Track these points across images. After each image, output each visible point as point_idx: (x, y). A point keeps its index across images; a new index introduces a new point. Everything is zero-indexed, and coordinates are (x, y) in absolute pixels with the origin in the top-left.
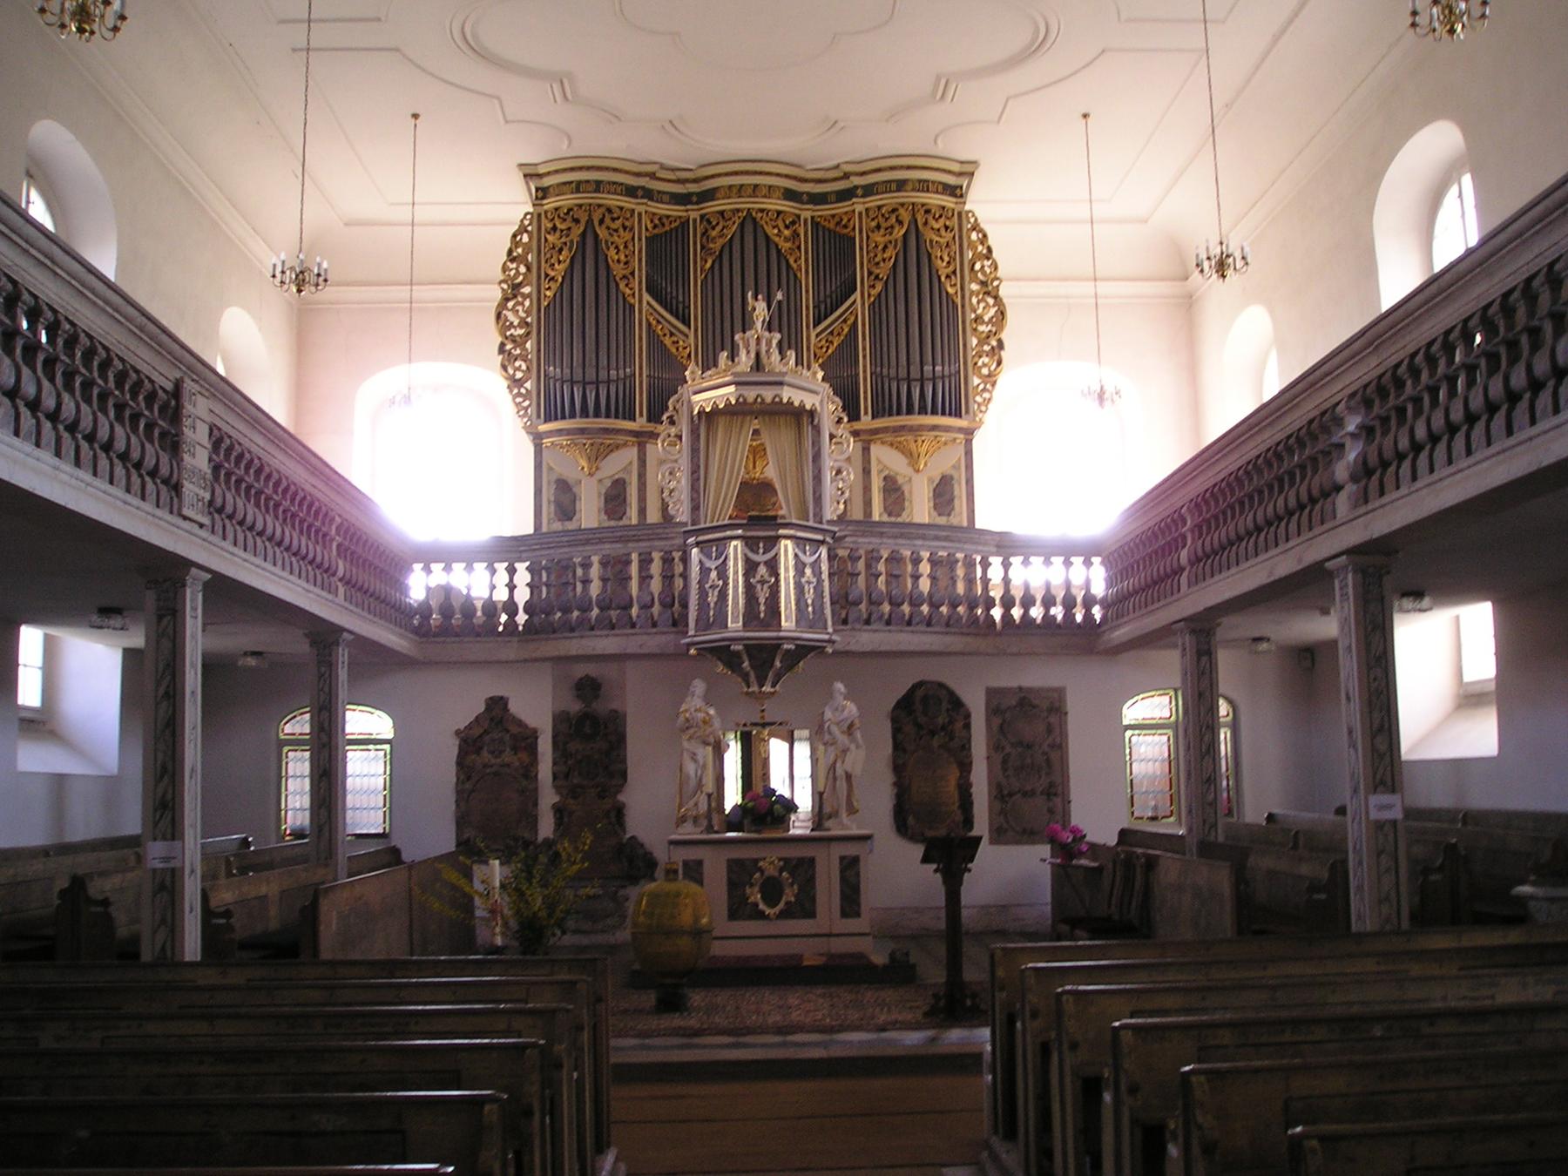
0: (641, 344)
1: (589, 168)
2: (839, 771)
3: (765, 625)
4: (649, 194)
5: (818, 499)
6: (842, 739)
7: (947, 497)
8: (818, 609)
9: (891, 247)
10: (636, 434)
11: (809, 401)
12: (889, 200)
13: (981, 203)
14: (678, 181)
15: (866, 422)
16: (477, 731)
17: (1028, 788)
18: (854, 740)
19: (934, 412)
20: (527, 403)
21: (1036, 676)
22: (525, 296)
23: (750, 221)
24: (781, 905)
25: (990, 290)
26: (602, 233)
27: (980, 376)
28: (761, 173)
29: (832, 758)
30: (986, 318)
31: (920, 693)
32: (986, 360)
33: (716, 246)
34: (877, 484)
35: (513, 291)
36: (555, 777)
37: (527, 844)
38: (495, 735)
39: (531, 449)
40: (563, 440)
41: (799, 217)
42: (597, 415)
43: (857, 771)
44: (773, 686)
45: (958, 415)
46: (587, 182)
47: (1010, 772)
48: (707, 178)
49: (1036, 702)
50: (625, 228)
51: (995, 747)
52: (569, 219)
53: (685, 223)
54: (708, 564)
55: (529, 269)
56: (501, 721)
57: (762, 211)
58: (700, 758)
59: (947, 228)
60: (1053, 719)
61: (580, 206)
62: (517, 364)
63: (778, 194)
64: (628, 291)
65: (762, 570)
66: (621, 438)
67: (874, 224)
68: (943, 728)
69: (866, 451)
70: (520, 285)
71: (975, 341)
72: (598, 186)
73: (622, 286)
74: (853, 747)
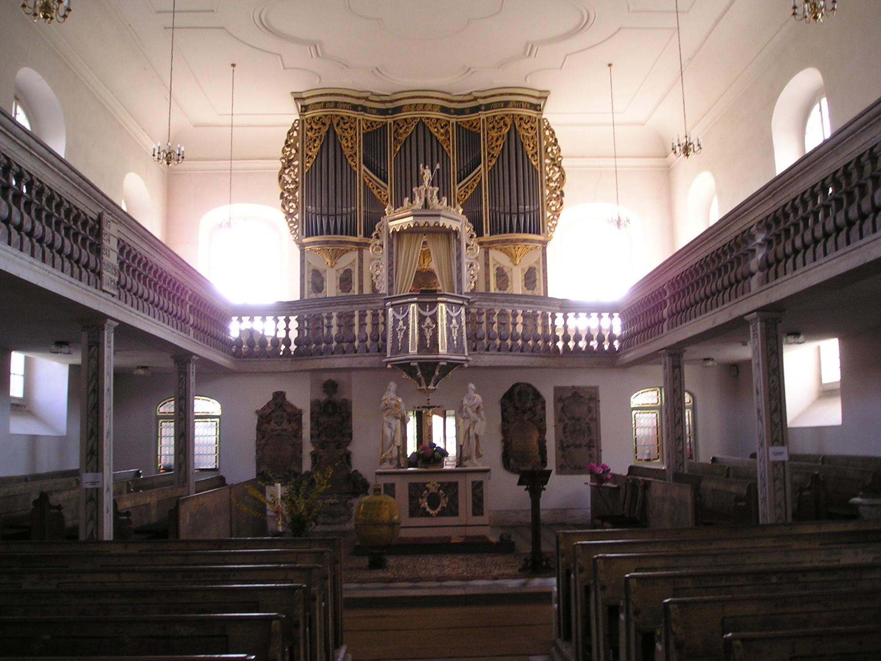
0: (360, 193)
1: (331, 95)
2: (472, 434)
3: (430, 351)
4: (365, 109)
5: (460, 281)
6: (473, 415)
7: (532, 279)
8: (460, 342)
9: (500, 139)
10: (357, 244)
11: (455, 226)
12: (499, 112)
13: (551, 114)
14: (381, 102)
15: (487, 237)
16: (268, 411)
17: (578, 443)
18: (480, 416)
19: (525, 232)
20: (296, 227)
21: (582, 380)
22: (295, 167)
23: (421, 124)
24: (439, 509)
25: (556, 163)
26: (338, 131)
27: (551, 211)
28: (427, 97)
29: (468, 426)
30: (554, 179)
31: (517, 390)
32: (554, 202)
33: (402, 138)
34: (493, 272)
35: (288, 164)
36: (312, 436)
37: (296, 475)
38: (278, 413)
39: (298, 252)
40: (317, 247)
41: (449, 122)
42: (335, 233)
43: (482, 433)
44: (435, 385)
45: (538, 233)
46: (330, 102)
47: (568, 434)
48: (397, 100)
49: (582, 395)
50: (351, 128)
51: (559, 420)
52: (320, 123)
53: (385, 126)
54: (398, 317)
55: (297, 151)
56: (281, 405)
57: (428, 118)
58: (393, 426)
59: (532, 128)
60: (592, 404)
61: (326, 116)
62: (291, 204)
63: (437, 109)
64: (353, 164)
65: (428, 320)
66: (349, 246)
67: (491, 126)
68: (530, 409)
69: (487, 253)
70: (292, 160)
71: (548, 192)
72: (336, 105)
73: (349, 161)
74: (479, 420)
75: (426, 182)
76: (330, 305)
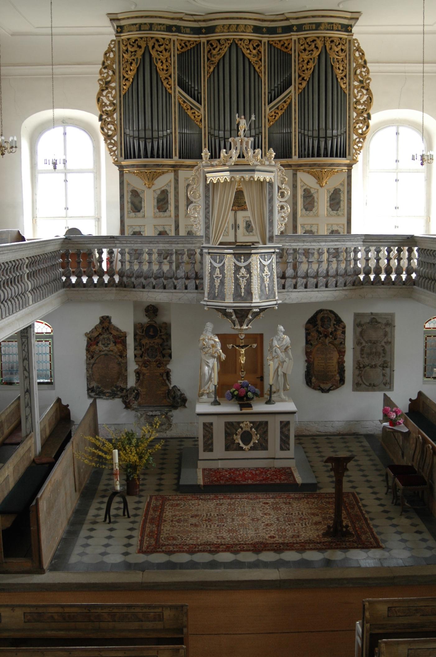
0: (175, 110)
1: (146, 17)
2: (280, 373)
3: (244, 300)
4: (178, 29)
5: (271, 223)
6: (282, 355)
7: (337, 200)
9: (311, 62)
10: (173, 166)
11: (268, 177)
12: (312, 34)
13: (359, 32)
14: (195, 21)
15: (295, 159)
16: (96, 334)
17: (373, 363)
20: (115, 148)
21: (380, 308)
22: (113, 88)
23: (234, 45)
24: (251, 444)
25: (365, 86)
27: (357, 134)
28: (241, 18)
29: (277, 365)
30: (362, 101)
31: (320, 316)
32: (361, 125)
33: (216, 60)
34: (300, 193)
35: (106, 85)
36: (135, 356)
37: (122, 390)
38: (105, 336)
39: (118, 172)
41: (261, 41)
43: (289, 373)
44: (247, 326)
45: (344, 156)
46: (145, 24)
47: (365, 356)
48: (211, 20)
49: (379, 320)
50: (166, 50)
52: (136, 46)
53: (199, 45)
55: (114, 73)
56: (108, 329)
57: (241, 40)
59: (342, 50)
60: (388, 329)
61: (141, 38)
62: (109, 126)
63: (250, 29)
64: (168, 86)
65: (243, 271)
66: (165, 169)
67: (302, 48)
68: (331, 333)
69: (295, 175)
71: (355, 115)
72: (151, 27)
73: (165, 83)
74: (287, 359)
75: (241, 133)
76: (151, 242)
